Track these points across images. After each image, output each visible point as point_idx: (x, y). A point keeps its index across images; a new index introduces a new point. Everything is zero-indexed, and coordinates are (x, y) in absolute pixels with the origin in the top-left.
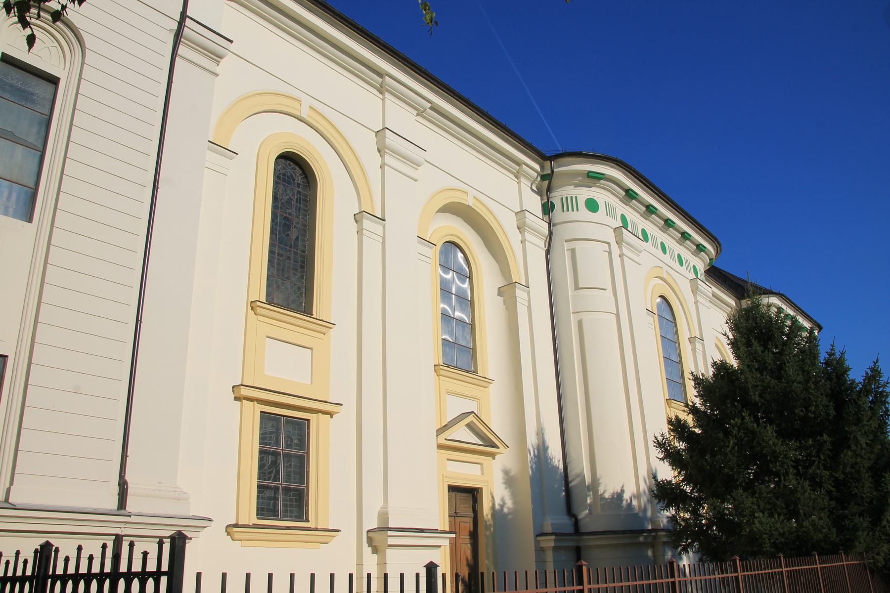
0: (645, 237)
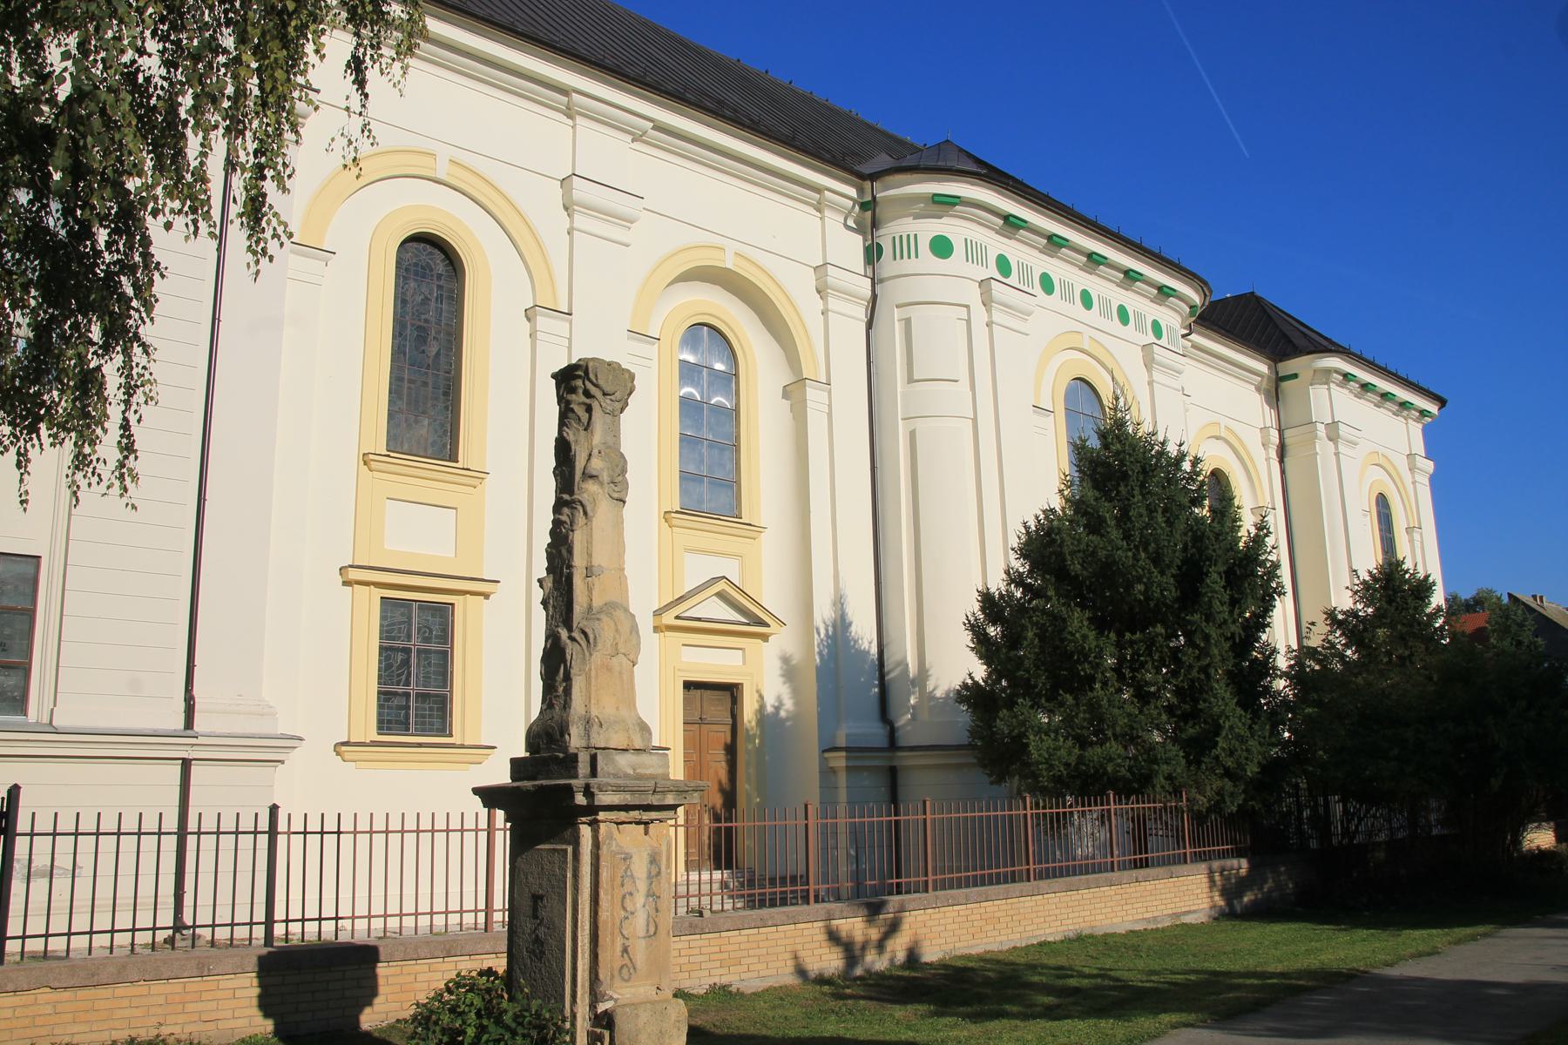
0: (1047, 284)
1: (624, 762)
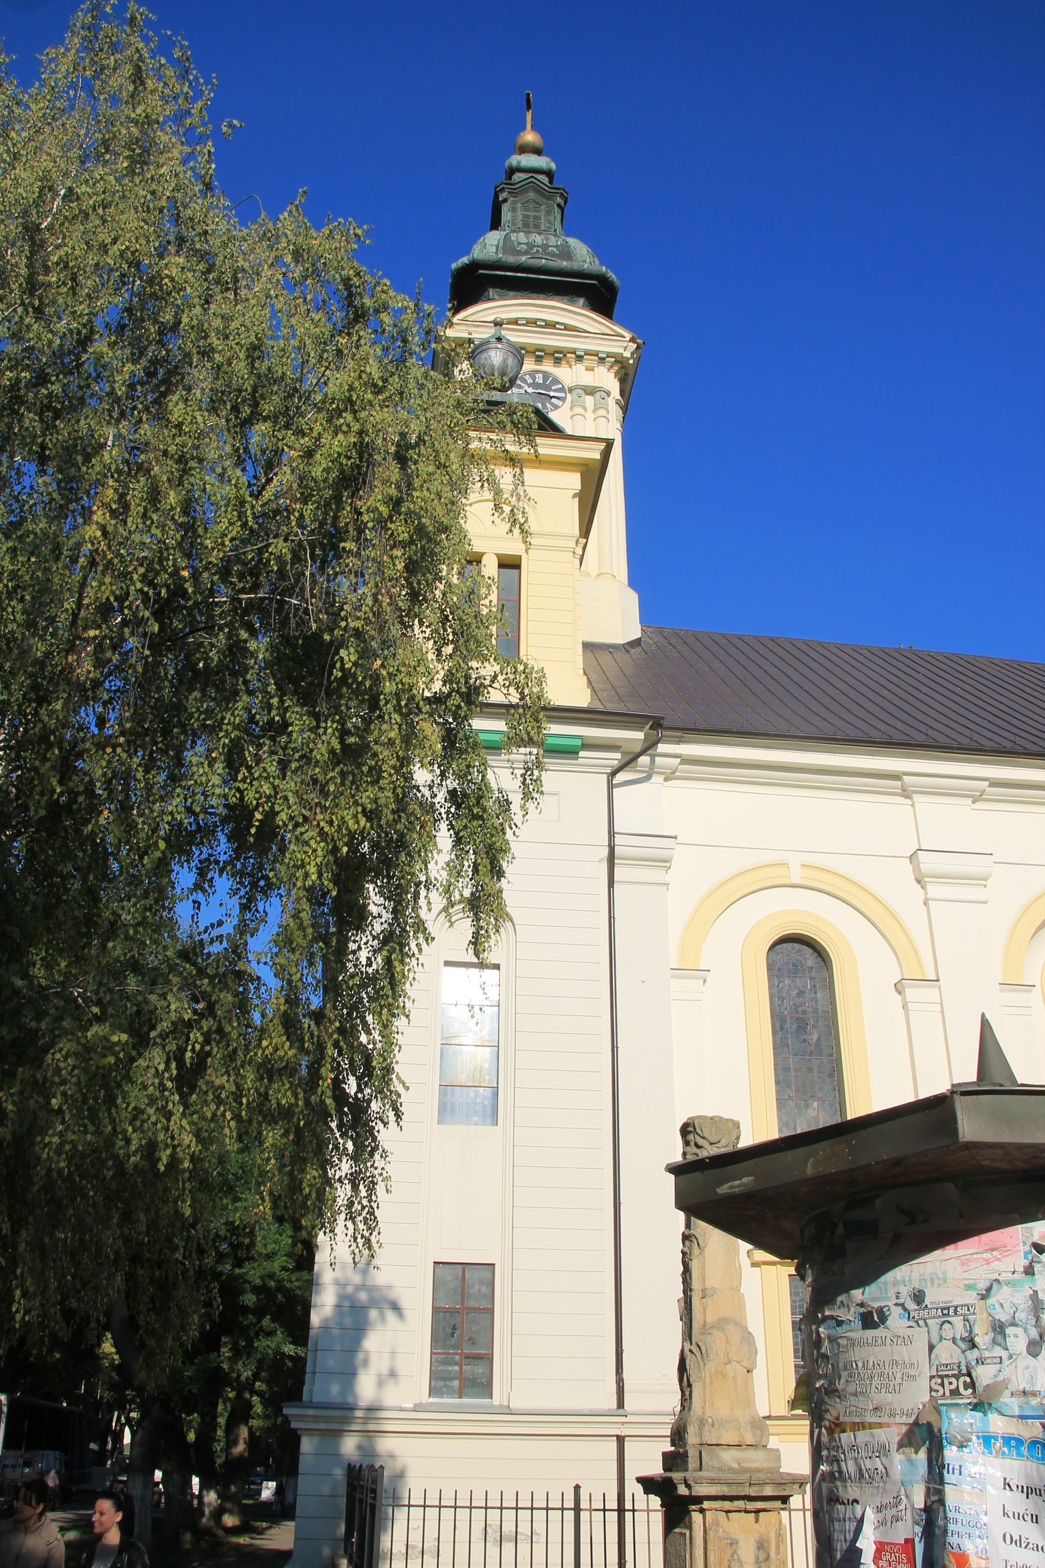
1: (728, 1457)
